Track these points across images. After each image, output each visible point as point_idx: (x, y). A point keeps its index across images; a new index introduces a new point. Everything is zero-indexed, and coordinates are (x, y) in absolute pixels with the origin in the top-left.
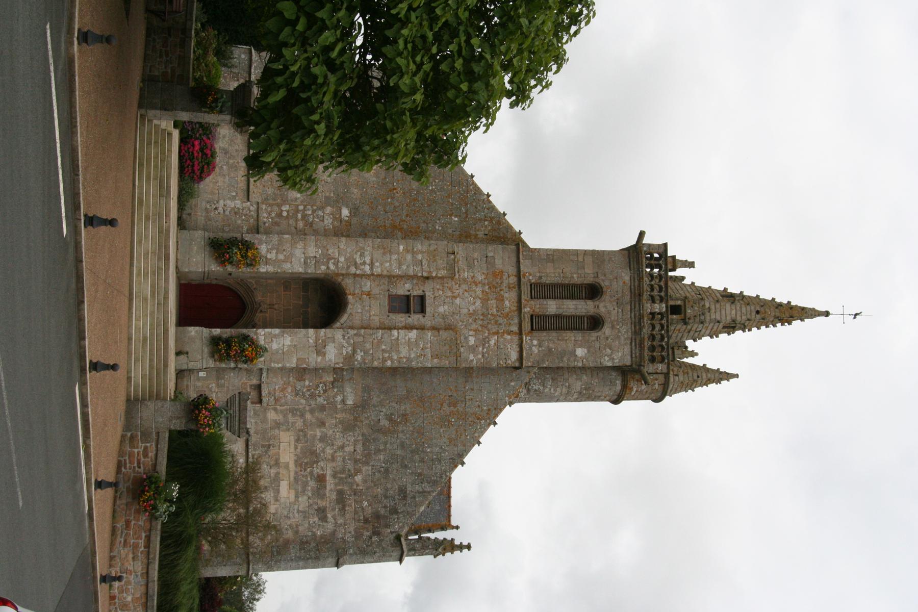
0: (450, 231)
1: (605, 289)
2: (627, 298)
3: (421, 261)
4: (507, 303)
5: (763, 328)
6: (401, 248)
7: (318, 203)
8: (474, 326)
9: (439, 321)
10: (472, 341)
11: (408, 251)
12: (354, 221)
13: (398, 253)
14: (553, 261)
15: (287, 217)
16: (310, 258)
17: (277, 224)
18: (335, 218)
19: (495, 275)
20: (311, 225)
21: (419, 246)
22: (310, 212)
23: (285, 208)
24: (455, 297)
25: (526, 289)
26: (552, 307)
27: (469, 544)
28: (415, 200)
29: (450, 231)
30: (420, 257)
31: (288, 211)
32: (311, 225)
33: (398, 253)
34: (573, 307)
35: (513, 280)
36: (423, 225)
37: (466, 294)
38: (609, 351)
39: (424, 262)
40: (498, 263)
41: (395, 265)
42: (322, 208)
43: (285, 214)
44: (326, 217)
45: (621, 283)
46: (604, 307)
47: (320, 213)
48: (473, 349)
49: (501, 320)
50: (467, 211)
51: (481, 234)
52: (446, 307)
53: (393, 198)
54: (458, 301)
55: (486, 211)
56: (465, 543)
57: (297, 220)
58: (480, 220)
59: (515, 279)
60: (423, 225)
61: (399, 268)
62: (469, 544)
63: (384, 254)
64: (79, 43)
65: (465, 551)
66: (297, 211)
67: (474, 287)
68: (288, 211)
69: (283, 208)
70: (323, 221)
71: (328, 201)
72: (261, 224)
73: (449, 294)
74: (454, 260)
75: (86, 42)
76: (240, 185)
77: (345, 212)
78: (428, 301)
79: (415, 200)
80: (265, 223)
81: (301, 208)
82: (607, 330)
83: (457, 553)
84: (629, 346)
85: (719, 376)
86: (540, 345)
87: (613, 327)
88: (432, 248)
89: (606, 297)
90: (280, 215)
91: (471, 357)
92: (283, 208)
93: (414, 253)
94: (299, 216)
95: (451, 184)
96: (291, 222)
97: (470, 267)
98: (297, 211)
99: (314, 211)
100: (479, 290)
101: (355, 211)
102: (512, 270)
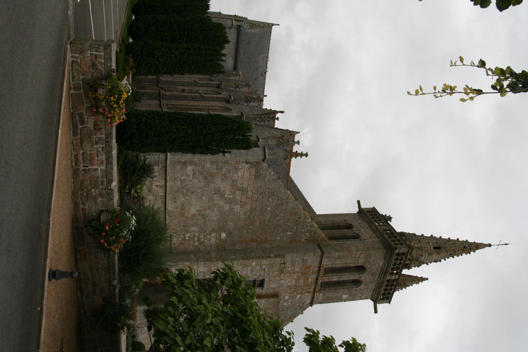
0: (285, 240)
1: (367, 269)
2: (379, 272)
3: (265, 269)
4: (310, 280)
5: (455, 257)
6: (254, 264)
7: (208, 232)
8: (289, 291)
9: (270, 291)
10: (287, 297)
11: (258, 265)
12: (228, 239)
13: (252, 266)
14: (341, 258)
15: (188, 240)
16: (200, 272)
17: (182, 244)
18: (217, 239)
19: (306, 268)
20: (203, 243)
21: (264, 262)
22: (202, 237)
23: (187, 235)
24: (281, 280)
25: (322, 270)
26: (335, 278)
27: (307, 153)
28: (266, 225)
29: (285, 240)
30: (264, 267)
31: (189, 237)
32: (203, 243)
33: (252, 266)
34: (347, 277)
35: (316, 269)
36: (269, 238)
37: (288, 278)
38: (360, 295)
39: (266, 269)
40: (310, 262)
41: (249, 272)
42: (210, 234)
43: (187, 238)
44: (212, 239)
45: (377, 266)
46: (364, 277)
47: (208, 237)
48: (287, 301)
49: (304, 288)
50: (297, 230)
51: (303, 240)
52: (275, 285)
53: (253, 226)
54: (282, 282)
55: (309, 227)
56: (304, 153)
57: (194, 241)
58: (304, 232)
59: (317, 269)
60: (269, 238)
61: (251, 273)
62: (307, 153)
63: (243, 267)
64: (50, 280)
65: (304, 157)
66: (195, 236)
67: (293, 274)
68: (189, 237)
69: (186, 236)
70: (210, 241)
71: (213, 230)
72: (173, 245)
73: (278, 278)
74: (284, 267)
75: (55, 278)
76: (160, 194)
77: (224, 235)
78: (266, 283)
79: (266, 225)
80: (175, 244)
81: (197, 235)
82: (362, 287)
83: (299, 158)
84: (372, 292)
85: (422, 279)
86: (323, 296)
87: (366, 285)
88: (272, 262)
89: (367, 273)
90: (184, 239)
91: (285, 304)
92: (186, 236)
93: (261, 265)
94: (196, 239)
95: (290, 215)
96: (191, 242)
97: (293, 265)
98: (195, 236)
99: (205, 236)
100: (295, 276)
101: (229, 234)
102: (316, 265)
